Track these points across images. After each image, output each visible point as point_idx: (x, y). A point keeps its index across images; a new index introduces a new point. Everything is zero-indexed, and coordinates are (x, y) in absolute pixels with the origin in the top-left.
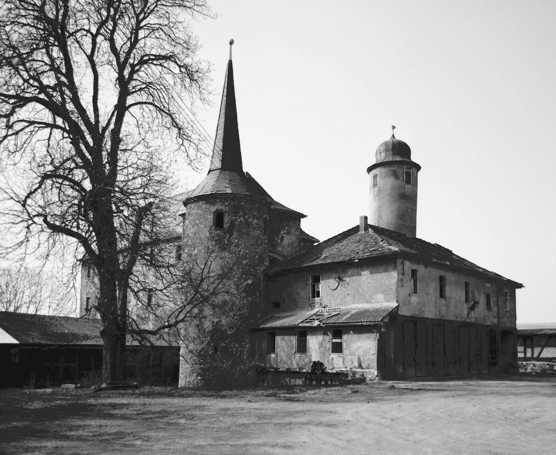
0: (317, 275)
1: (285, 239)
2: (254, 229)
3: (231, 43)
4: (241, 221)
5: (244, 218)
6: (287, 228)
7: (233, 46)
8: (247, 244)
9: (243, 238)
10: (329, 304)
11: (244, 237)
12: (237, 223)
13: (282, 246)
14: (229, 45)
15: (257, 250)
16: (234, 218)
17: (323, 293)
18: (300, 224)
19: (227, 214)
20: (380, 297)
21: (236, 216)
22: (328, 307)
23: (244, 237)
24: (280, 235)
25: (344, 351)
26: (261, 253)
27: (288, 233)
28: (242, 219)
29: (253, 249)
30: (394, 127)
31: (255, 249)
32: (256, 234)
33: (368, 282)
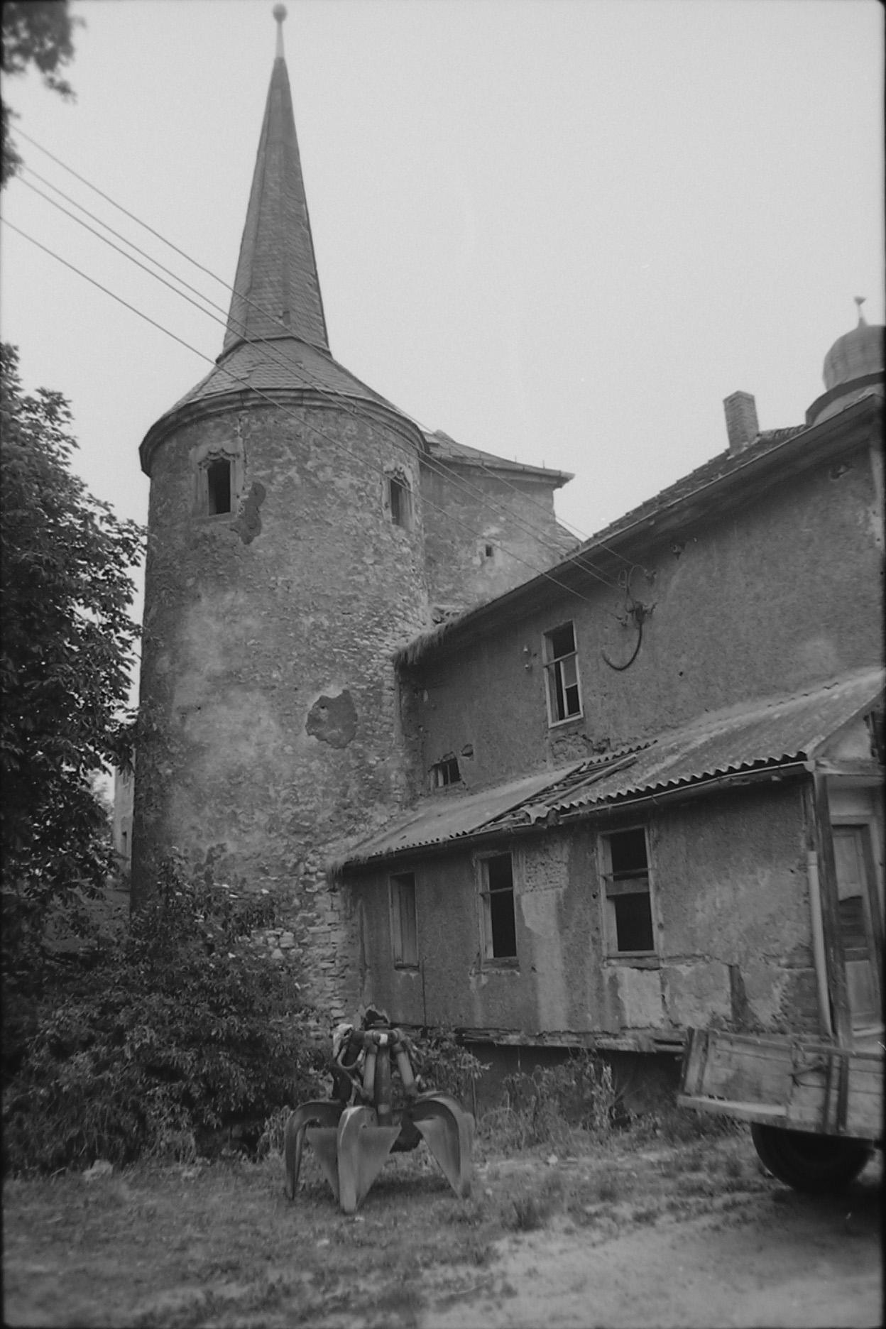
0: (562, 623)
1: (498, 553)
2: (344, 505)
3: (280, 15)
4: (290, 479)
5: (301, 471)
6: (502, 519)
7: (285, 23)
8: (314, 557)
9: (299, 539)
10: (613, 735)
11: (303, 532)
12: (273, 489)
13: (488, 578)
14: (274, 23)
15: (362, 579)
16: (261, 473)
17: (588, 690)
18: (551, 505)
19: (239, 463)
20: (819, 648)
21: (270, 466)
22: (613, 744)
23: (303, 532)
24: (479, 542)
25: (659, 937)
26: (380, 588)
27: (509, 533)
28: (292, 473)
29: (342, 574)
30: (860, 301)
31: (349, 574)
32: (354, 522)
33: (758, 598)
